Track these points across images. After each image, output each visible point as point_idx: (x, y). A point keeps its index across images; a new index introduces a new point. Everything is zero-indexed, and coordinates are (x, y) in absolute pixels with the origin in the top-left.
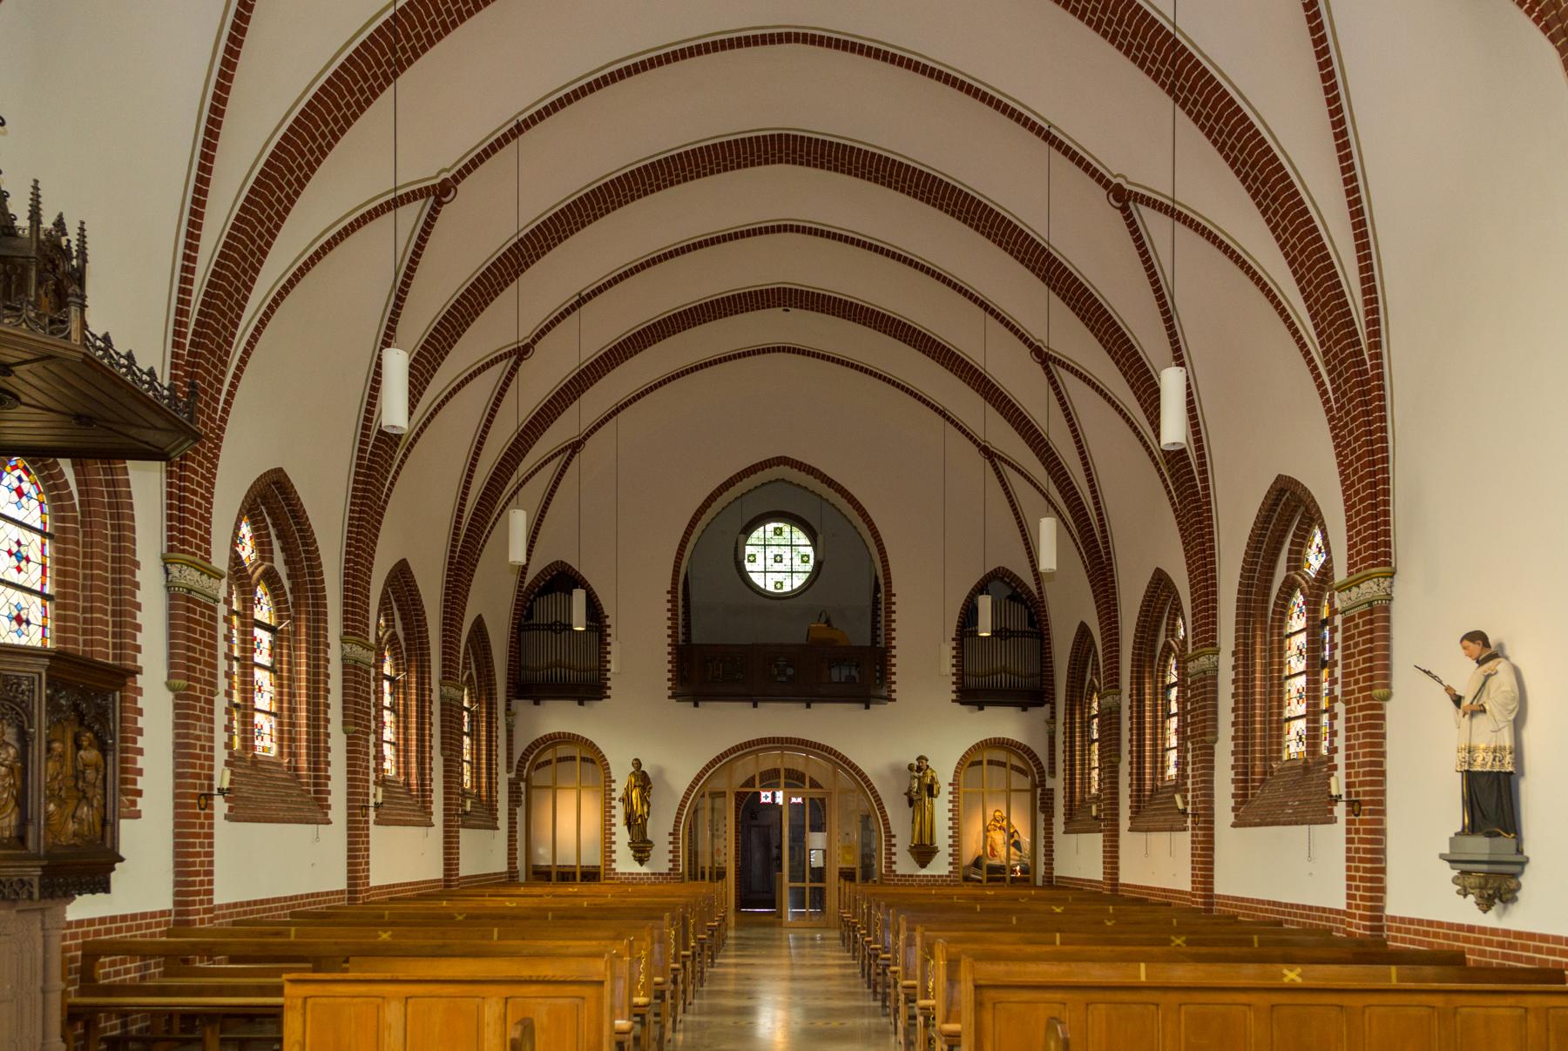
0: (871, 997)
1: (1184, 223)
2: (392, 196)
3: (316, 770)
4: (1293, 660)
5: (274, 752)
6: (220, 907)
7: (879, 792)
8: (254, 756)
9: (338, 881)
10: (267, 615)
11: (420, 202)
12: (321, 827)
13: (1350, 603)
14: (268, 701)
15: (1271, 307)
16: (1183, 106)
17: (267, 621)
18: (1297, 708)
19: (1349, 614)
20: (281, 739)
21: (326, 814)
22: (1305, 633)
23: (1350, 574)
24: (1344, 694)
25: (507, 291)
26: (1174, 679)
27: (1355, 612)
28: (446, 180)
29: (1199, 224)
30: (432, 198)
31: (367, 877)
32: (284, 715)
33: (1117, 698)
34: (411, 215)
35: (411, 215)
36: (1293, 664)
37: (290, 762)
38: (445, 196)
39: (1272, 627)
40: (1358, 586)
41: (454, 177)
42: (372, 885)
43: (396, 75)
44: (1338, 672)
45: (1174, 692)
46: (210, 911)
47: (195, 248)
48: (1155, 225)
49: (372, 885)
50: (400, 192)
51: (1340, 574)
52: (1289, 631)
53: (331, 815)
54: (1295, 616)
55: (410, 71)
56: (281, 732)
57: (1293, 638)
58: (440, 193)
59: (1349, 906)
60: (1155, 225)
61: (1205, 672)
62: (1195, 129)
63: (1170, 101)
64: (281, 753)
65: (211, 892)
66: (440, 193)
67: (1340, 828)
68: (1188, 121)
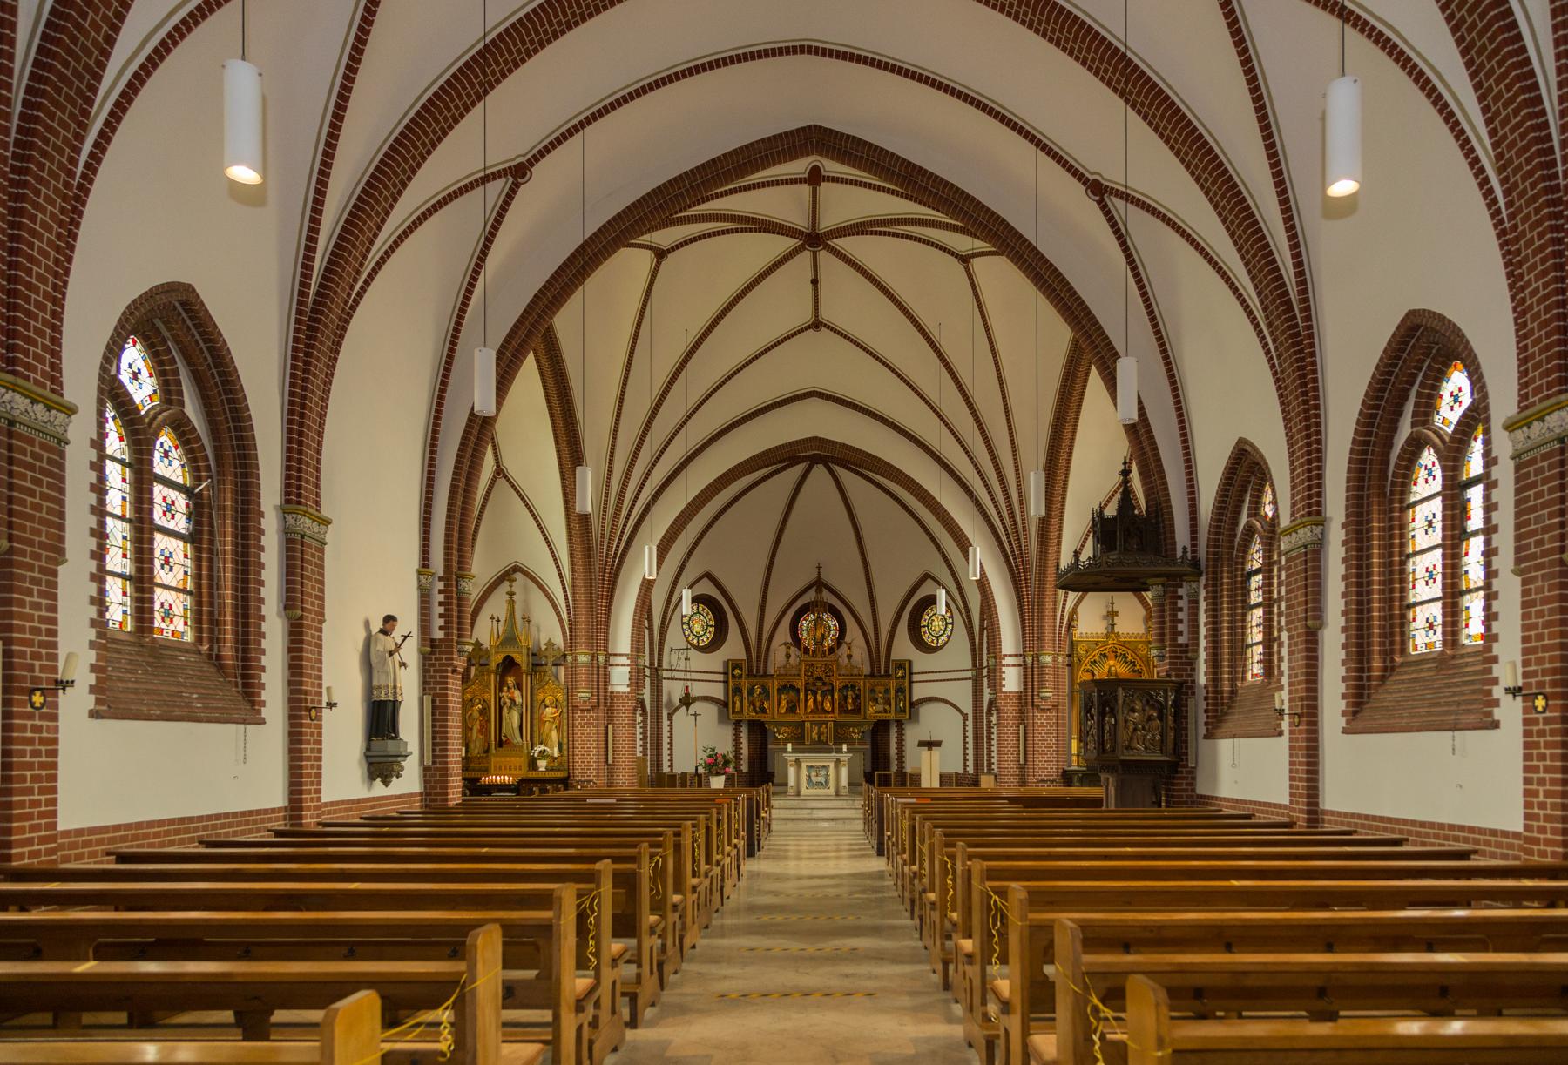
0: (908, 914)
1: (1137, 205)
2: (482, 174)
3: (245, 659)
4: (1419, 534)
5: (189, 638)
6: (67, 833)
7: (467, 316)
8: (154, 640)
9: (274, 796)
10: (179, 471)
11: (503, 180)
12: (249, 727)
13: (1530, 443)
14: (181, 576)
15: (1222, 282)
16: (1133, 107)
17: (180, 481)
18: (1256, 635)
19: (1290, 555)
20: (199, 621)
21: (259, 712)
22: (1439, 499)
23: (1522, 409)
24: (1287, 623)
25: (469, 117)
26: (1256, 565)
27: (1294, 554)
28: (522, 163)
29: (1155, 209)
30: (511, 179)
31: (318, 791)
32: (203, 594)
33: (1318, 530)
34: (496, 188)
35: (496, 188)
36: (1418, 539)
37: (211, 649)
38: (523, 177)
39: (1392, 493)
40: (1542, 419)
41: (529, 160)
42: (324, 800)
43: (486, 93)
44: (1283, 605)
45: (1257, 581)
46: (53, 839)
47: (318, 222)
48: (1117, 205)
49: (324, 800)
50: (488, 172)
51: (1285, 521)
52: (1412, 499)
53: (265, 712)
54: (1421, 481)
55: (498, 89)
56: (199, 612)
57: (1418, 508)
58: (519, 172)
59: (1291, 802)
60: (1117, 205)
61: (1305, 547)
62: (1145, 125)
63: (1121, 102)
64: (199, 640)
65: (54, 814)
66: (519, 172)
67: (1284, 741)
68: (1139, 119)
